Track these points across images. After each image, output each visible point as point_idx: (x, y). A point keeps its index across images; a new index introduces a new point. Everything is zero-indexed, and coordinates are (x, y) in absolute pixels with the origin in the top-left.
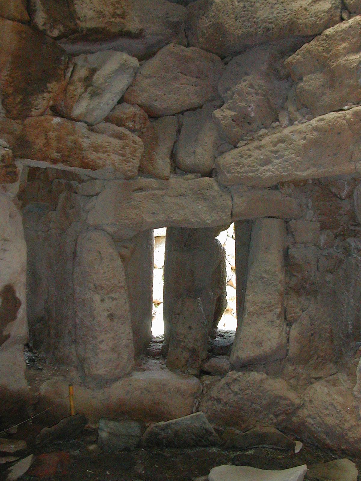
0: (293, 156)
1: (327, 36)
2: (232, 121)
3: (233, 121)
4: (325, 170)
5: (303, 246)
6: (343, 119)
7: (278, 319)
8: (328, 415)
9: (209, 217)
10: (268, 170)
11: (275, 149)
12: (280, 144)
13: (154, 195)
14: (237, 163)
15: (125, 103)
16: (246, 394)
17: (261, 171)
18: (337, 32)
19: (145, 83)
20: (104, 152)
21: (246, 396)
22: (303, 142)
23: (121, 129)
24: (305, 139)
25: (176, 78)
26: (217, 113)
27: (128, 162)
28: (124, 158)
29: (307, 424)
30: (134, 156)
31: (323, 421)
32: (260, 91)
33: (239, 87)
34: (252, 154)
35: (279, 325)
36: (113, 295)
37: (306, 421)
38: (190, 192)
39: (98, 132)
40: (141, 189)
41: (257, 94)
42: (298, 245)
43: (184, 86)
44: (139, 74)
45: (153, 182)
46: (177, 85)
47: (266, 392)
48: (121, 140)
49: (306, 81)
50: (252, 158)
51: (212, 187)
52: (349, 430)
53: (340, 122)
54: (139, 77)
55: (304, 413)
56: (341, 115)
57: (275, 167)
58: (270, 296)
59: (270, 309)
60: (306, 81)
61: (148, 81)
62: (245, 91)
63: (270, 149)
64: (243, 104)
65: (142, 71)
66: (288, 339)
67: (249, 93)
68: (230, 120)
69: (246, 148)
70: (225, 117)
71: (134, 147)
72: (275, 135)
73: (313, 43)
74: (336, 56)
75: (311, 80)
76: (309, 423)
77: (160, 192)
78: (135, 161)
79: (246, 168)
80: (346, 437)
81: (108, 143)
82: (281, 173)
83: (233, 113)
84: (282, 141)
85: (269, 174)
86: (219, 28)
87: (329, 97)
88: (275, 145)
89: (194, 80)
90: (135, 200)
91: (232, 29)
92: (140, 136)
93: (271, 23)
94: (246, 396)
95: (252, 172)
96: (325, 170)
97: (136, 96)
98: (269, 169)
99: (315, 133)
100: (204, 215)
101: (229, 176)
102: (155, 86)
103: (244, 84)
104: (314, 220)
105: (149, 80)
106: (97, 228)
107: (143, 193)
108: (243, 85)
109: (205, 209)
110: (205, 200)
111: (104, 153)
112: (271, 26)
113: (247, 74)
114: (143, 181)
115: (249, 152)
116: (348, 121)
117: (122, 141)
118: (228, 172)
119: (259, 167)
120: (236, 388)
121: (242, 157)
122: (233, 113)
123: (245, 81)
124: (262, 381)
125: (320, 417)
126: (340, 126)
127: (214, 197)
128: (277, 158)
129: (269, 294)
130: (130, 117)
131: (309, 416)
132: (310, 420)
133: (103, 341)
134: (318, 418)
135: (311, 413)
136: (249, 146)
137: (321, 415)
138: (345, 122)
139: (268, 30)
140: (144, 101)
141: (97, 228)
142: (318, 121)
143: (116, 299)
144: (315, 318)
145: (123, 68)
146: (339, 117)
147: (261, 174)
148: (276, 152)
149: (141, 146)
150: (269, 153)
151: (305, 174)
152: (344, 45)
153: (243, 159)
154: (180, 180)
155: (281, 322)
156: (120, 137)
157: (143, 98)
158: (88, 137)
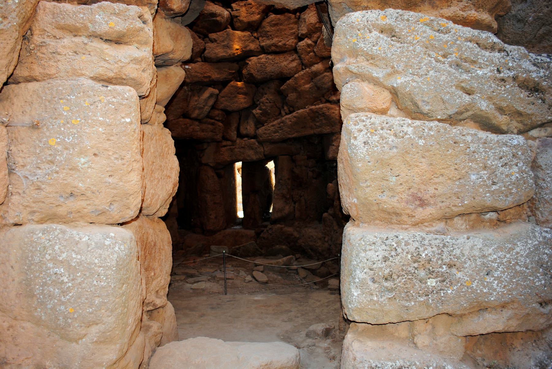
1: (295, 78)
3: (261, 115)
10: (277, 135)
13: (230, 148)
18: (299, 76)
20: (206, 132)
22: (290, 123)
23: (213, 121)
24: (291, 121)
26: (254, 111)
33: (262, 100)
40: (225, 146)
41: (270, 103)
45: (229, 143)
51: (255, 144)
55: (300, 241)
61: (224, 99)
64: (264, 108)
65: (220, 94)
66: (295, 210)
67: (267, 103)
70: (257, 113)
73: (290, 80)
74: (300, 86)
83: (261, 112)
85: (277, 137)
86: (251, 75)
91: (257, 76)
93: (273, 73)
95: (271, 136)
99: (295, 119)
101: (261, 138)
102: (227, 101)
103: (264, 99)
107: (226, 148)
108: (263, 99)
110: (253, 149)
112: (272, 74)
113: (266, 94)
114: (224, 143)
116: (307, 113)
118: (261, 137)
120: (270, 232)
121: (266, 130)
122: (261, 112)
127: (256, 148)
128: (280, 130)
132: (303, 244)
136: (269, 125)
139: (272, 75)
145: (211, 95)
148: (280, 127)
150: (277, 128)
151: (293, 136)
152: (303, 81)
156: (213, 124)
157: (222, 106)
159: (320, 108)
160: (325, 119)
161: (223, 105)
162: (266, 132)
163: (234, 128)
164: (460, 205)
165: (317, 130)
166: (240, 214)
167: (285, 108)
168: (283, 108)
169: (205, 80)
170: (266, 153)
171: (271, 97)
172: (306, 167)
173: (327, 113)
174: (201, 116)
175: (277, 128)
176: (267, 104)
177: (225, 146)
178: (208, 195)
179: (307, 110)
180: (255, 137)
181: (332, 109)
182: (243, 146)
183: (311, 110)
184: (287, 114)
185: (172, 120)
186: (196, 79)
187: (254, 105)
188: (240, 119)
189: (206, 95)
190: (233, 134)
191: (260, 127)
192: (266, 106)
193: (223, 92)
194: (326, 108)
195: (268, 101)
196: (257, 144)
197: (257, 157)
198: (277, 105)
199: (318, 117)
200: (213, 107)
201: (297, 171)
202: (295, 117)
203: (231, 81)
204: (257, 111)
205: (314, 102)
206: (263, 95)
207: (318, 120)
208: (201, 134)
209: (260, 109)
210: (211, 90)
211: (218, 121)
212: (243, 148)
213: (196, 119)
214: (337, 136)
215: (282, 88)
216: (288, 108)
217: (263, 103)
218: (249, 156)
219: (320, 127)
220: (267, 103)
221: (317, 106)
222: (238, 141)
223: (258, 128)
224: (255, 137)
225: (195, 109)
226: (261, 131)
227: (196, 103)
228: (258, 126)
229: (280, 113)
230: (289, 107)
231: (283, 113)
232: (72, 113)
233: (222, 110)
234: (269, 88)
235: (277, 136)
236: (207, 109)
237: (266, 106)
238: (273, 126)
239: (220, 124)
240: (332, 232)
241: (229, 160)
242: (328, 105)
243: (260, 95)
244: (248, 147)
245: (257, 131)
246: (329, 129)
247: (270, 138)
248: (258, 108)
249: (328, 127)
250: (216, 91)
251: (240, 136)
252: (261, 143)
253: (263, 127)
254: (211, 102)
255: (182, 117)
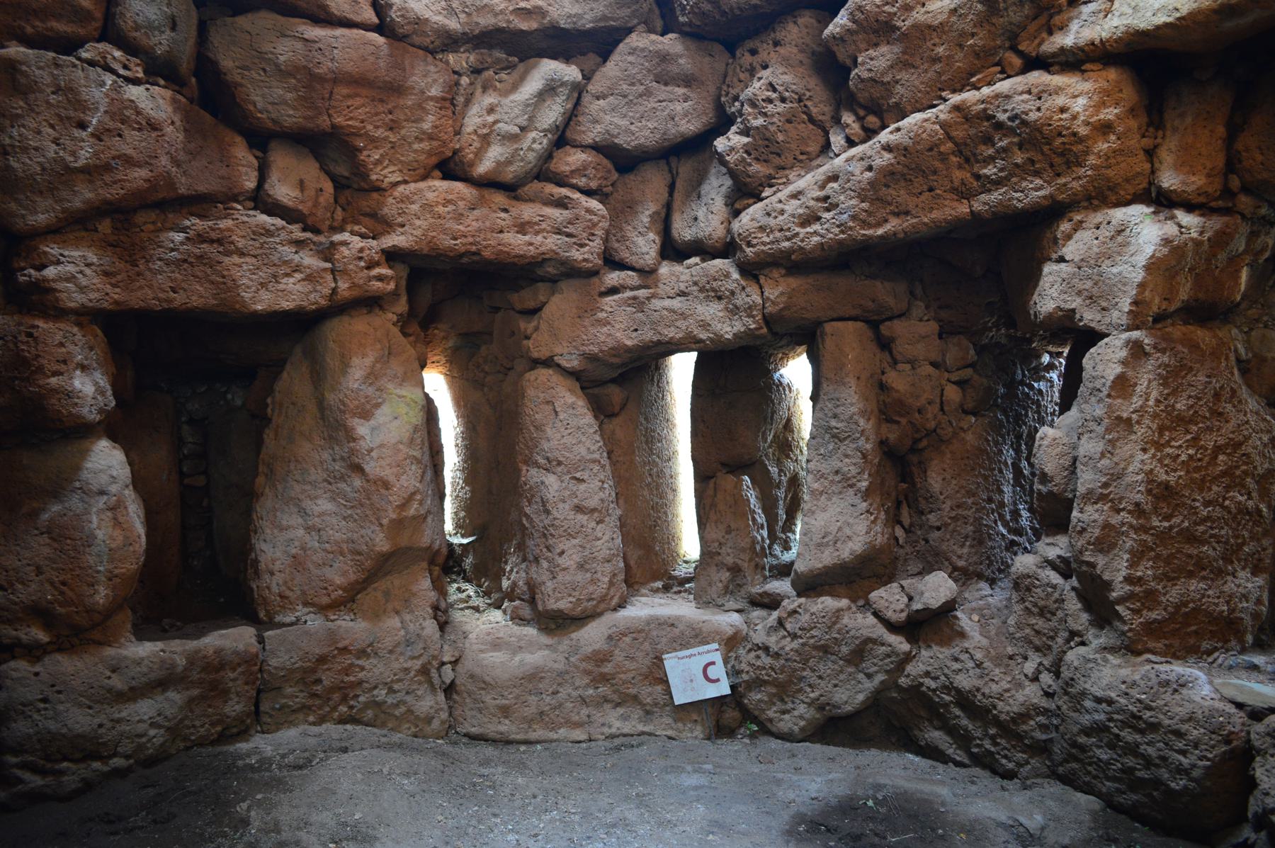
0: (854, 202)
2: (745, 155)
4: (914, 221)
5: (908, 367)
6: (934, 123)
7: (865, 501)
8: (960, 670)
9: (729, 329)
11: (821, 194)
12: (831, 185)
13: (635, 298)
14: (761, 227)
15: (568, 147)
16: (813, 637)
17: (801, 236)
19: (593, 107)
21: (812, 641)
22: (868, 175)
23: (564, 191)
24: (870, 168)
25: (648, 93)
27: (582, 246)
28: (574, 240)
29: (924, 689)
30: (593, 235)
31: (951, 683)
32: (787, 94)
33: (749, 92)
34: (786, 207)
35: (868, 511)
36: (578, 475)
37: (922, 684)
38: (695, 288)
39: (526, 201)
40: (613, 291)
42: (900, 366)
43: (664, 104)
44: (584, 94)
45: (629, 277)
46: (652, 104)
47: (847, 632)
48: (567, 209)
49: (863, 64)
50: (786, 215)
51: (727, 275)
52: (998, 699)
53: (928, 130)
54: (586, 98)
56: (929, 115)
57: (825, 226)
58: (847, 460)
59: (850, 482)
60: (863, 64)
62: (760, 98)
63: (814, 196)
64: (759, 122)
65: (590, 87)
67: (770, 101)
68: (741, 153)
69: (774, 199)
70: (732, 149)
71: (590, 220)
72: (821, 170)
75: (872, 59)
76: (928, 688)
77: (642, 293)
78: (594, 244)
79: (778, 234)
80: (995, 712)
81: (542, 216)
82: (836, 235)
84: (834, 178)
85: (816, 239)
87: (909, 83)
88: (823, 187)
89: (681, 91)
90: (603, 310)
92: (58, 139)
94: (812, 641)
95: (788, 239)
96: (914, 221)
97: (584, 132)
98: (815, 232)
99: (887, 156)
100: (719, 326)
104: (926, 318)
105: (602, 101)
106: (549, 363)
107: (616, 297)
108: (756, 88)
109: (721, 314)
110: (720, 298)
111: (537, 233)
114: (614, 278)
115: (780, 206)
116: (943, 125)
117: (567, 212)
118: (749, 244)
119: (798, 229)
121: (769, 214)
122: (746, 140)
123: (760, 79)
124: (839, 612)
125: (946, 675)
126: (930, 135)
127: (733, 293)
128: (828, 210)
129: (847, 456)
130: (578, 170)
131: (927, 674)
132: (928, 682)
133: (563, 552)
134: (943, 678)
135: (929, 669)
136: (779, 195)
137: (946, 671)
138: (938, 127)
140: (597, 139)
141: (549, 363)
142: (891, 133)
143: (583, 481)
144: (942, 497)
145: (550, 89)
146: (926, 120)
147: (802, 241)
148: (826, 198)
149: (603, 217)
150: (812, 203)
151: (880, 232)
153: (771, 219)
154: (678, 268)
155: (871, 505)
156: (561, 203)
157: (592, 133)
158: (506, 211)
159: (997, 96)
160: (1021, 146)
161: (599, 128)
162: (772, 222)
163: (646, 220)
164: (222, 403)
165: (984, 197)
166: (689, 544)
167: (848, 118)
168: (837, 120)
169: (524, 26)
170: (770, 309)
171: (788, 78)
172: (934, 364)
173: (1033, 116)
174: (512, 168)
175: (812, 203)
176: (770, 108)
177: (613, 291)
178: (551, 480)
179: (941, 111)
180: (728, 248)
181: (1058, 91)
182: (682, 286)
183: (957, 108)
184: (851, 143)
185: (397, 184)
186: (486, 21)
187: (723, 123)
188: (672, 188)
189: (533, 85)
190: (645, 245)
191: (749, 206)
192: (765, 115)
193: (598, 76)
194: (1029, 92)
195: (774, 95)
196: (736, 276)
197: (738, 327)
198: (814, 110)
199: (988, 140)
200: (561, 139)
201: (898, 381)
202: (887, 148)
203: (629, 31)
204: (730, 142)
205: (973, 75)
206: (752, 72)
207: (991, 151)
208: (517, 243)
209: (745, 132)
210: (549, 68)
211: (588, 193)
212: (682, 294)
213: (489, 183)
214: (1078, 217)
215: (827, 32)
216: (860, 119)
217: (753, 104)
218: (705, 325)
219: (998, 183)
220: (770, 101)
221: (986, 91)
222: (665, 269)
223: (736, 213)
224: (728, 248)
225: (486, 140)
226: (751, 216)
227: (490, 119)
228: (737, 206)
229: (827, 146)
230: (862, 113)
231: (837, 140)
232: (1146, 518)
233: (596, 148)
234: (777, 44)
235: (813, 237)
236: (535, 142)
237: (765, 115)
238: (795, 196)
239: (594, 204)
240: (1060, 640)
241: (629, 343)
242: (1037, 77)
243: (742, 76)
244: (702, 290)
245: (736, 226)
246: (1037, 189)
247: (787, 244)
248: (734, 129)
249: (1038, 182)
250: (571, 72)
251: (673, 250)
252: (751, 271)
253: (760, 205)
254: (552, 114)
255: (437, 173)
